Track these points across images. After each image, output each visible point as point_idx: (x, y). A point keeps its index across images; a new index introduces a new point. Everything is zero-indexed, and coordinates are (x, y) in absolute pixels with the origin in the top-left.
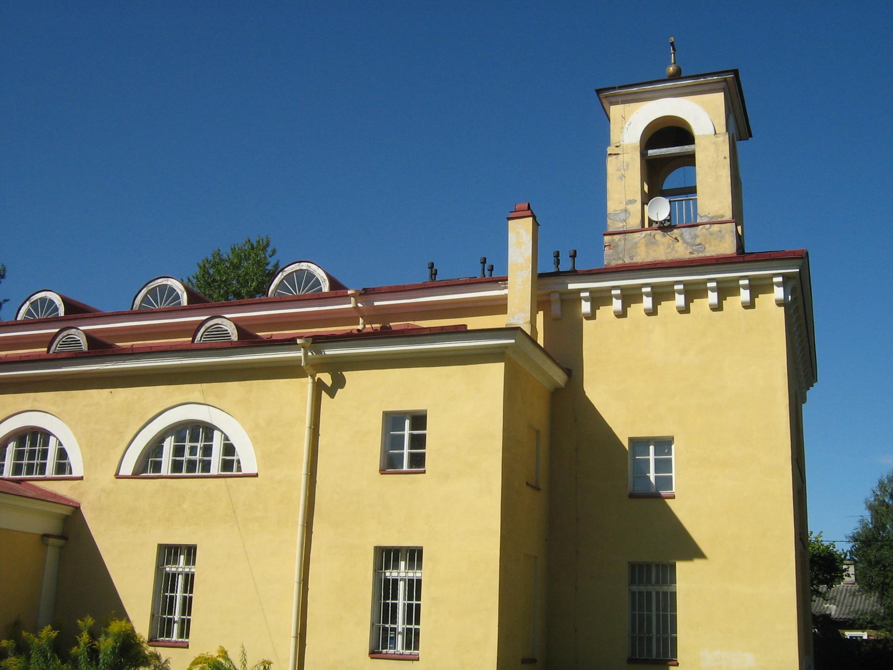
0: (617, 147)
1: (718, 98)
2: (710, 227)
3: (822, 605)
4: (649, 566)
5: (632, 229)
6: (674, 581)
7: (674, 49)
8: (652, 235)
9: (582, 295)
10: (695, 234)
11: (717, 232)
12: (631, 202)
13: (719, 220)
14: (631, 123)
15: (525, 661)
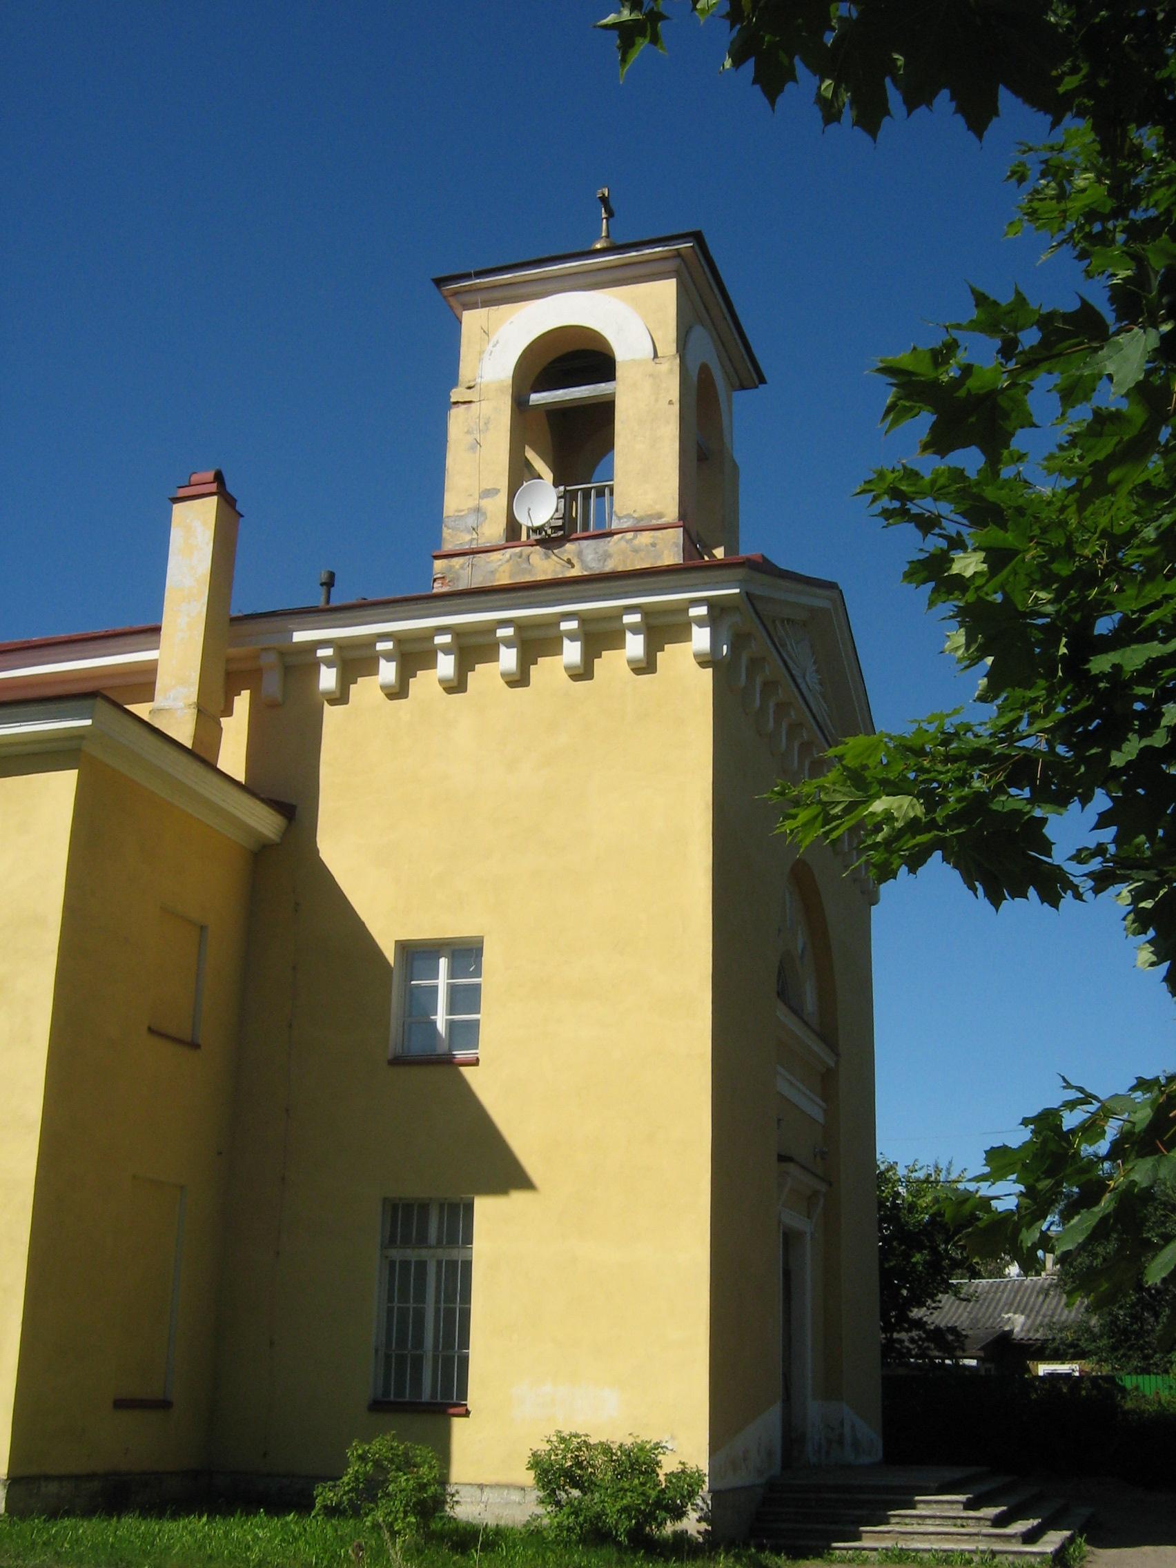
0: (470, 388)
1: (665, 291)
2: (635, 537)
3: (999, 1315)
4: (424, 1207)
5: (488, 545)
6: (468, 1239)
7: (610, 214)
8: (524, 556)
9: (321, 653)
10: (606, 551)
11: (646, 545)
12: (489, 493)
13: (654, 522)
14: (497, 342)
15: (121, 1404)
